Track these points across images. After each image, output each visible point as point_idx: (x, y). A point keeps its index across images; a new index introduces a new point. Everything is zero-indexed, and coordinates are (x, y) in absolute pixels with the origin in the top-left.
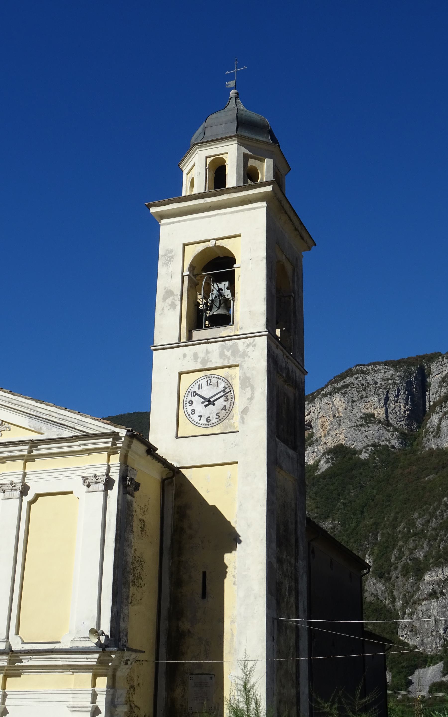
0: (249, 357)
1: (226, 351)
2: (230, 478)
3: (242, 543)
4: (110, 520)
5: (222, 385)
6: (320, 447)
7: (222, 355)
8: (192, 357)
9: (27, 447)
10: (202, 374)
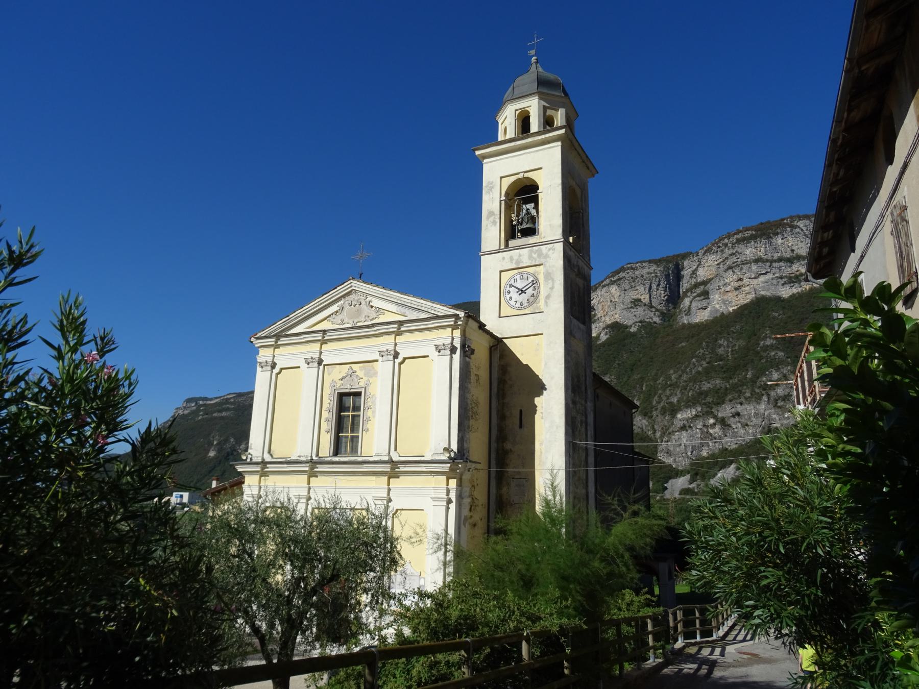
3: (547, 390)
5: (531, 279)
6: (601, 324)
7: (530, 257)
9: (396, 326)
10: (516, 271)
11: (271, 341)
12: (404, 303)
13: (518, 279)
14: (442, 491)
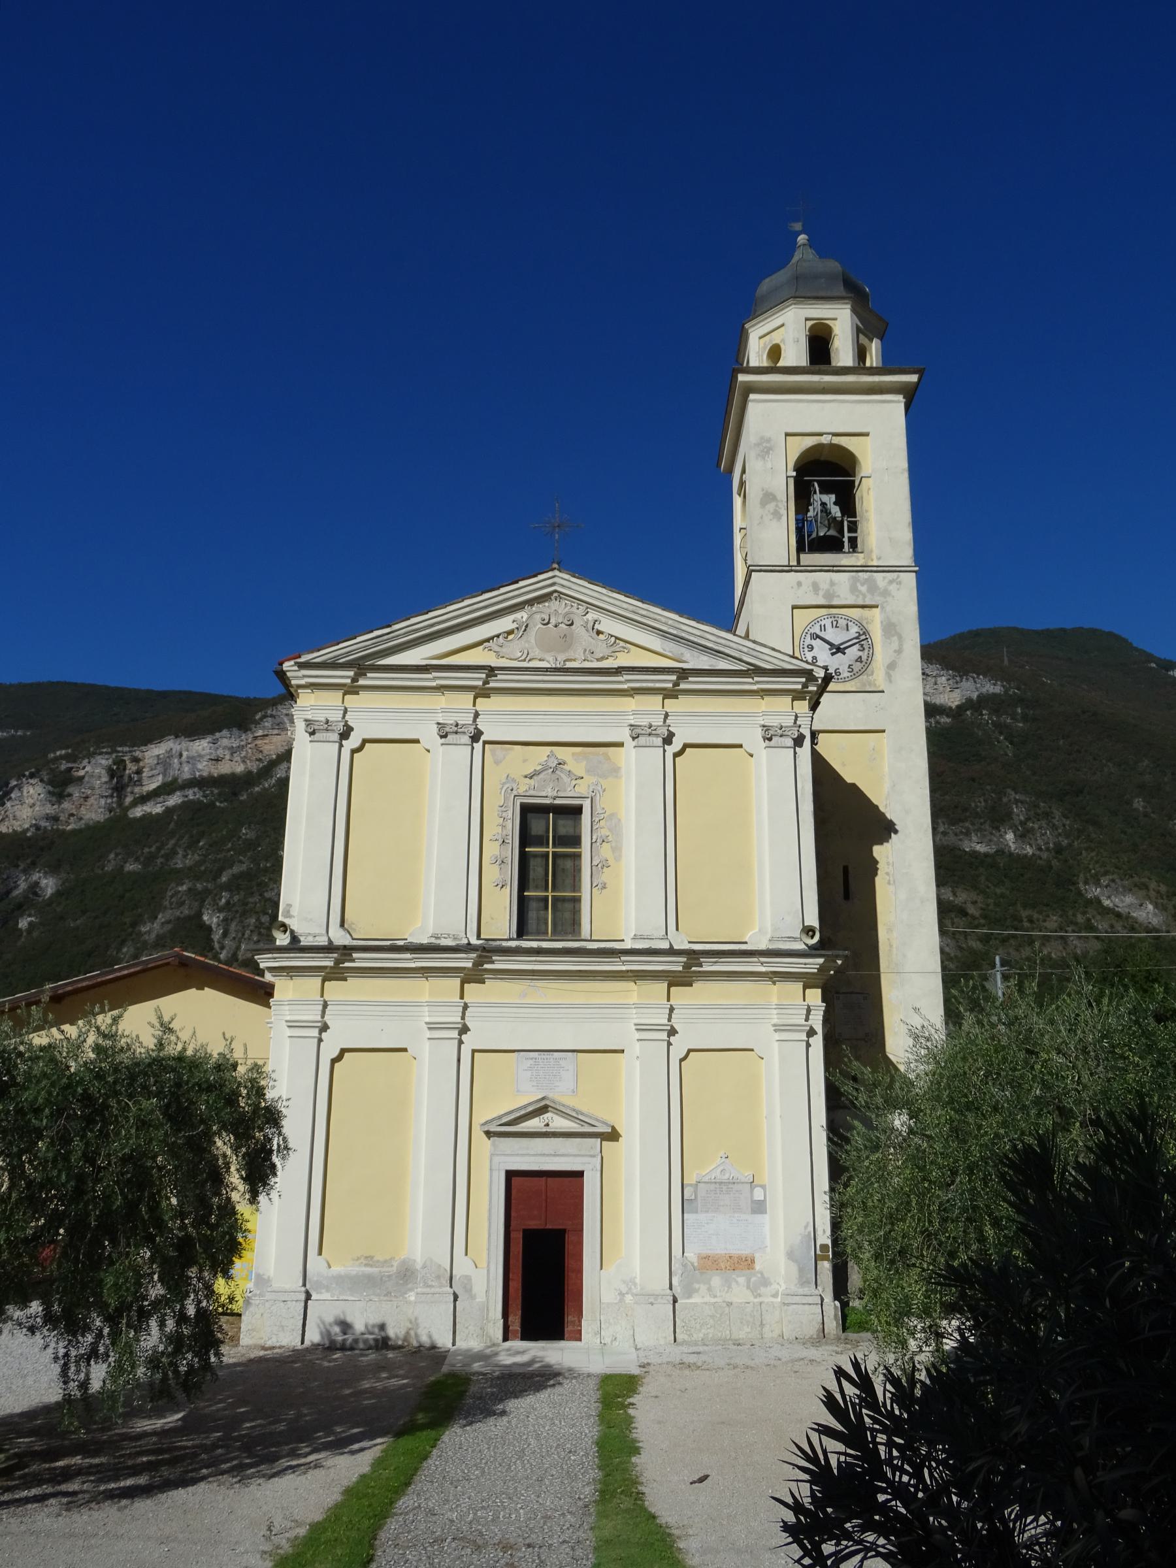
0: (893, 597)
1: (858, 584)
2: (874, 749)
3: (899, 834)
4: (803, 787)
5: (854, 630)
7: (854, 589)
8: (811, 588)
9: (674, 678)
10: (824, 611)
11: (344, 676)
12: (684, 635)
13: (829, 626)
14: (799, 1017)
